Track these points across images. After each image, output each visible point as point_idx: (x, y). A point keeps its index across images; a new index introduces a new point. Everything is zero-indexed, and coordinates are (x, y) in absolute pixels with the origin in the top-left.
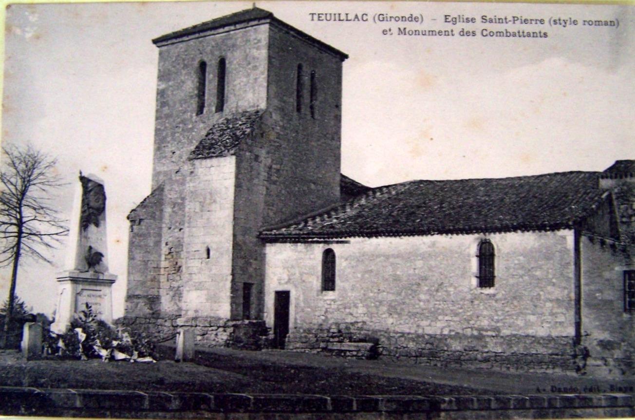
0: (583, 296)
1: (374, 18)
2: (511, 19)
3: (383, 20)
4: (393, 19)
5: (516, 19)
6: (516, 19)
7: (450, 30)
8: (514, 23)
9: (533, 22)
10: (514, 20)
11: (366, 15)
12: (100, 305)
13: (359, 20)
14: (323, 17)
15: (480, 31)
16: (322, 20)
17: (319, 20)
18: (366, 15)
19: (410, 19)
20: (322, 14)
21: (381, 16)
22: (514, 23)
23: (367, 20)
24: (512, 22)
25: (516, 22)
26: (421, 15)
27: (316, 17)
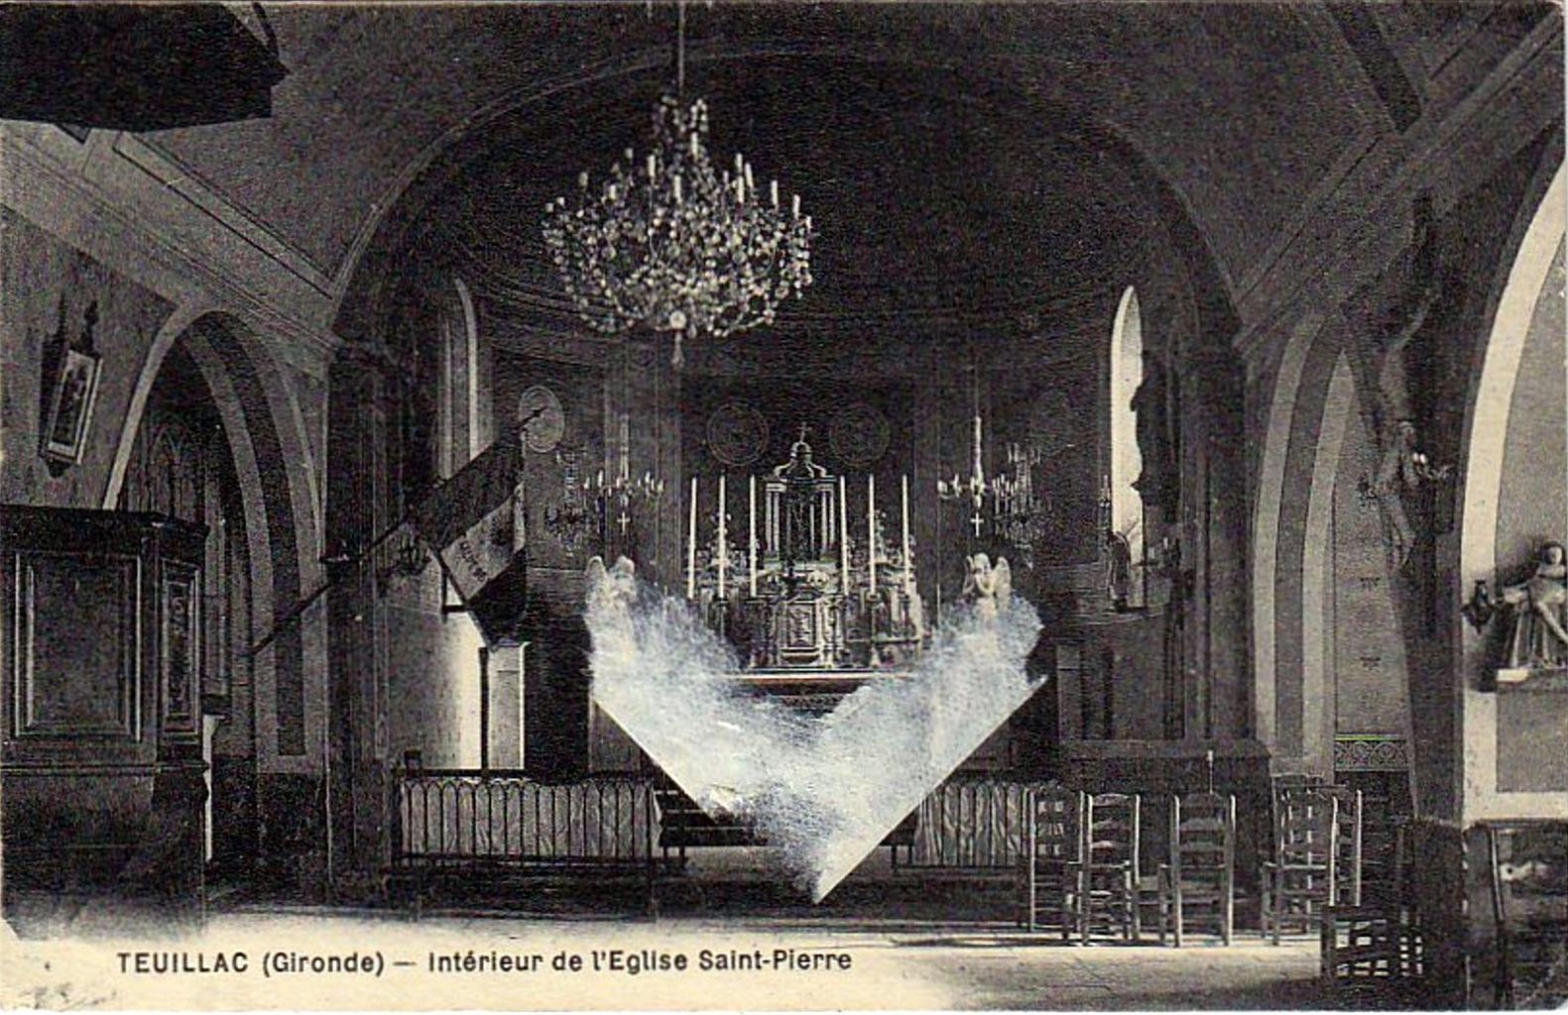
0: (490, 749)
1: (267, 956)
2: (771, 958)
3: (286, 968)
4: (307, 966)
5: (780, 956)
6: (780, 956)
7: (752, 954)
8: (776, 967)
9: (822, 963)
10: (777, 960)
11: (244, 956)
12: (1480, 583)
13: (226, 970)
14: (149, 963)
15: (552, 959)
16: (146, 970)
17: (139, 970)
18: (244, 956)
19: (351, 964)
20: (146, 955)
21: (280, 959)
22: (776, 967)
23: (245, 968)
24: (772, 964)
25: (780, 964)
26: (379, 955)
27: (131, 962)
